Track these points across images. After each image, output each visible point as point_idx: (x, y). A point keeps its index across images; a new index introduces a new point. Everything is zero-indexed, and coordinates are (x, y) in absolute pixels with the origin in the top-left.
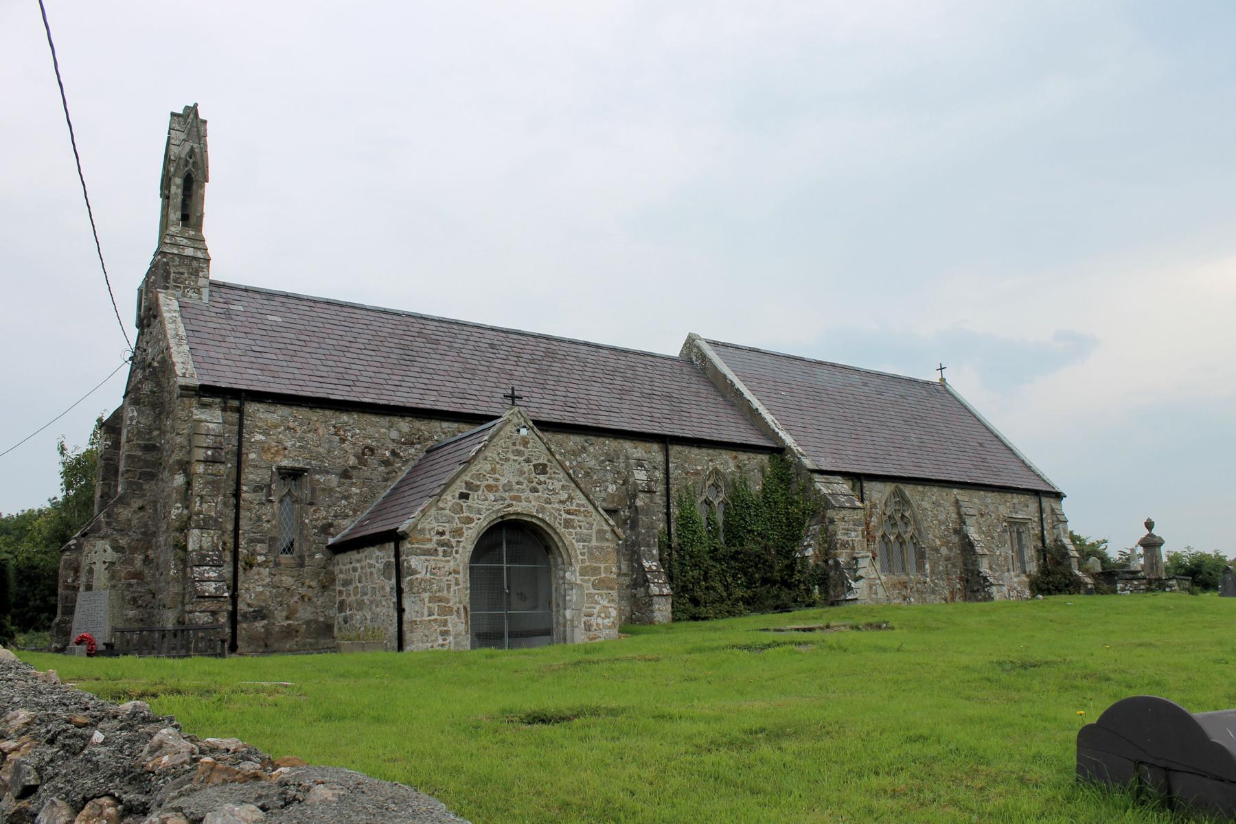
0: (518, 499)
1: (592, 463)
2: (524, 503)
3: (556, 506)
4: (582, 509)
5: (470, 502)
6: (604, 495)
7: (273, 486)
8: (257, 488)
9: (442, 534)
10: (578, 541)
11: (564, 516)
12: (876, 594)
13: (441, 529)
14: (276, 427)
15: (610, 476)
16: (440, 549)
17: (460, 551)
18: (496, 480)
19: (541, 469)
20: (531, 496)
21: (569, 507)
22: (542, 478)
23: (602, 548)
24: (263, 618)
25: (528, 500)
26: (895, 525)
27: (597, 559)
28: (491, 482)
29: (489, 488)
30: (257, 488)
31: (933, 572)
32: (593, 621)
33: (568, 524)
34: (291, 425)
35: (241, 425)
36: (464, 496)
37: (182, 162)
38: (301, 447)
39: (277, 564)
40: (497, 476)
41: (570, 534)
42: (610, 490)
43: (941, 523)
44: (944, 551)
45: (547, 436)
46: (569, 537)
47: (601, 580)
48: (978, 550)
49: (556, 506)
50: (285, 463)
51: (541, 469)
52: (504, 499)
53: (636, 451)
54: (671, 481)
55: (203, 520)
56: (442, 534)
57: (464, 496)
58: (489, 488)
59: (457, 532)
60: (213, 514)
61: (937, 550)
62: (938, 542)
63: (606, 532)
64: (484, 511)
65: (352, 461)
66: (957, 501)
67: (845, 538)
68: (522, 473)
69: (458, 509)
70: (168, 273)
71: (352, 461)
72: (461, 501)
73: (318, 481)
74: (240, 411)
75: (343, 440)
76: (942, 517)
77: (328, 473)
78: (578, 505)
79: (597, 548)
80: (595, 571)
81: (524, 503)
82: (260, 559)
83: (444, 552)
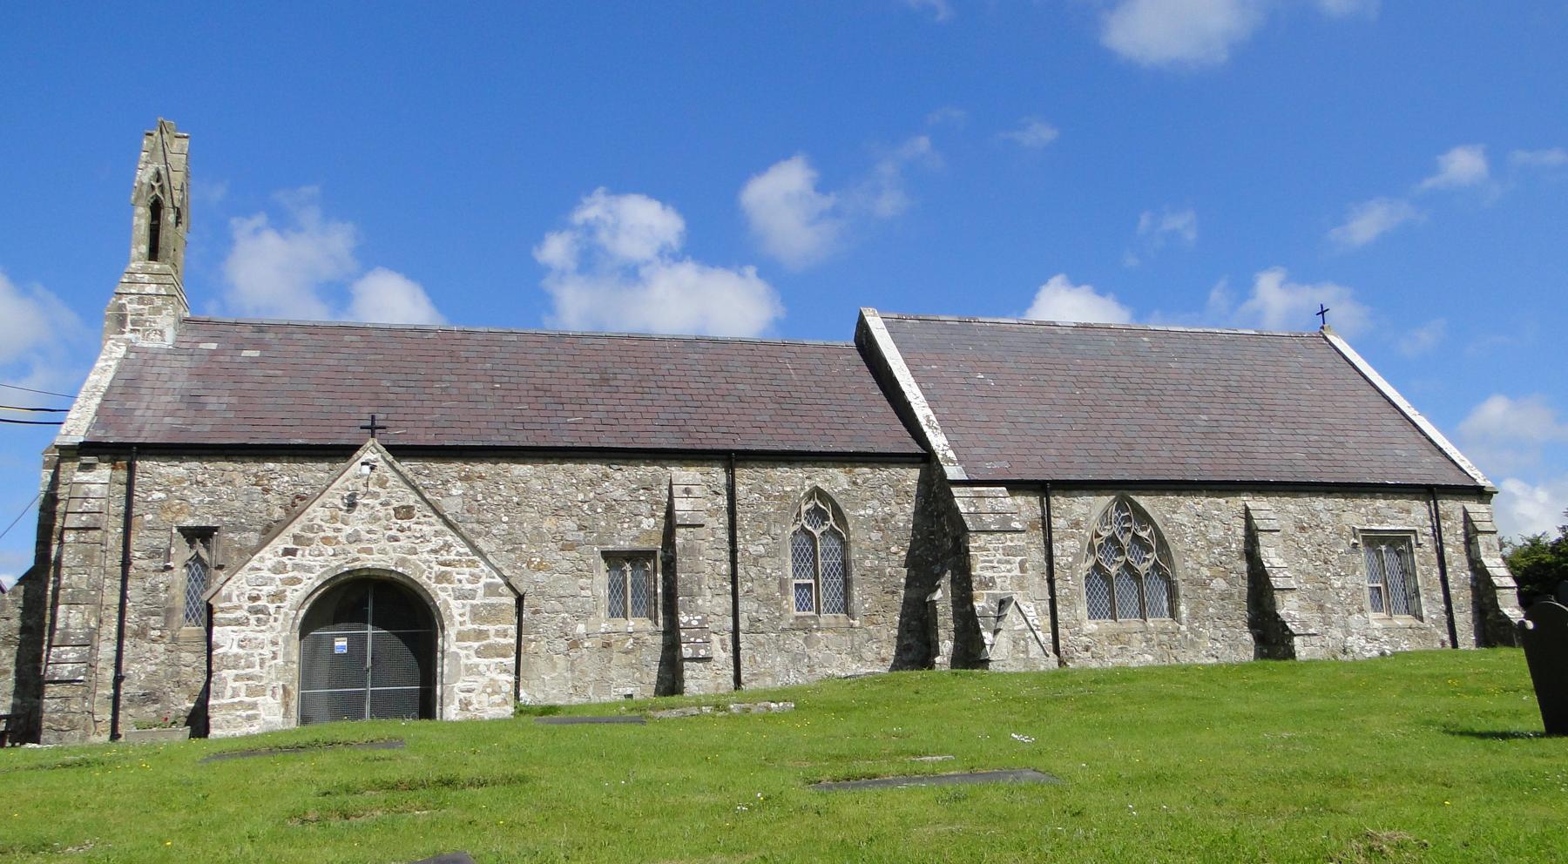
0: (369, 551)
1: (618, 493)
2: (376, 556)
3: (426, 556)
4: (464, 558)
5: (298, 559)
6: (635, 531)
7: (173, 550)
8: (154, 553)
9: (257, 598)
10: (457, 598)
11: (437, 568)
12: (1026, 651)
13: (254, 593)
14: (179, 482)
15: (645, 509)
16: (253, 618)
17: (281, 617)
18: (338, 530)
19: (405, 512)
20: (389, 546)
21: (445, 557)
22: (405, 523)
23: (492, 605)
24: (155, 701)
25: (383, 551)
26: (1121, 552)
27: (485, 620)
28: (331, 534)
29: (326, 540)
30: (154, 553)
31: (1194, 616)
32: (473, 697)
33: (442, 578)
34: (199, 478)
35: (130, 484)
36: (288, 552)
37: (145, 188)
38: (211, 502)
39: (174, 639)
40: (339, 525)
41: (444, 590)
42: (644, 526)
43: (1211, 544)
44: (1220, 584)
45: (405, 466)
46: (443, 596)
47: (489, 646)
48: (1277, 582)
49: (426, 556)
50: (190, 522)
51: (405, 512)
52: (345, 552)
53: (684, 475)
54: (738, 508)
55: (72, 594)
56: (257, 598)
57: (288, 552)
58: (326, 540)
59: (278, 597)
60: (84, 586)
61: (1204, 585)
62: (1205, 572)
63: (499, 586)
64: (316, 568)
65: (278, 513)
66: (1247, 510)
67: (988, 574)
68: (377, 519)
69: (279, 569)
70: (125, 316)
71: (278, 513)
72: (285, 559)
73: (231, 539)
74: (131, 469)
75: (266, 491)
76: (1217, 534)
77: (245, 530)
78: (458, 554)
79: (484, 606)
80: (480, 635)
81: (376, 556)
82: (155, 634)
83: (258, 620)
